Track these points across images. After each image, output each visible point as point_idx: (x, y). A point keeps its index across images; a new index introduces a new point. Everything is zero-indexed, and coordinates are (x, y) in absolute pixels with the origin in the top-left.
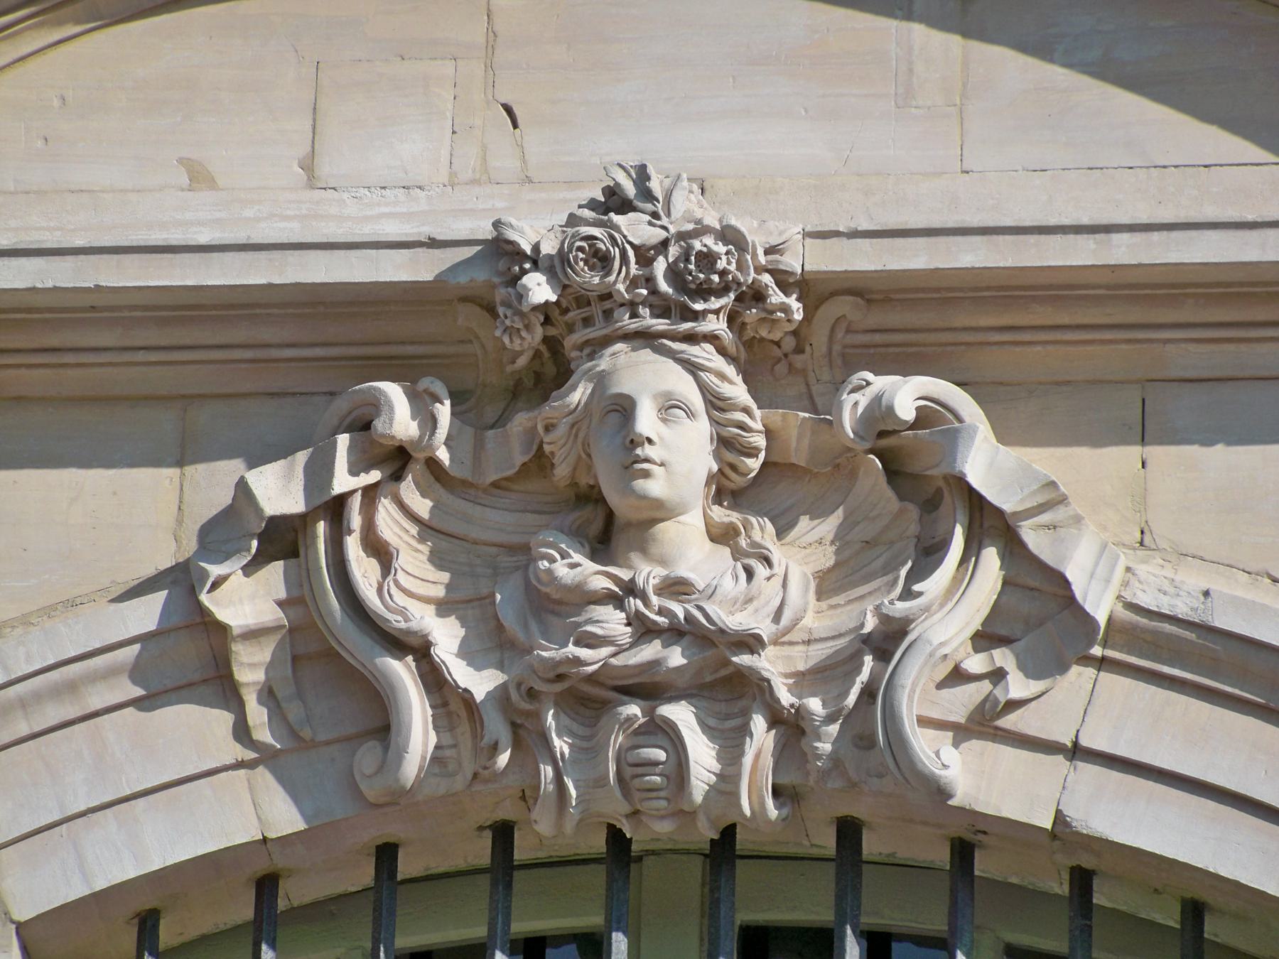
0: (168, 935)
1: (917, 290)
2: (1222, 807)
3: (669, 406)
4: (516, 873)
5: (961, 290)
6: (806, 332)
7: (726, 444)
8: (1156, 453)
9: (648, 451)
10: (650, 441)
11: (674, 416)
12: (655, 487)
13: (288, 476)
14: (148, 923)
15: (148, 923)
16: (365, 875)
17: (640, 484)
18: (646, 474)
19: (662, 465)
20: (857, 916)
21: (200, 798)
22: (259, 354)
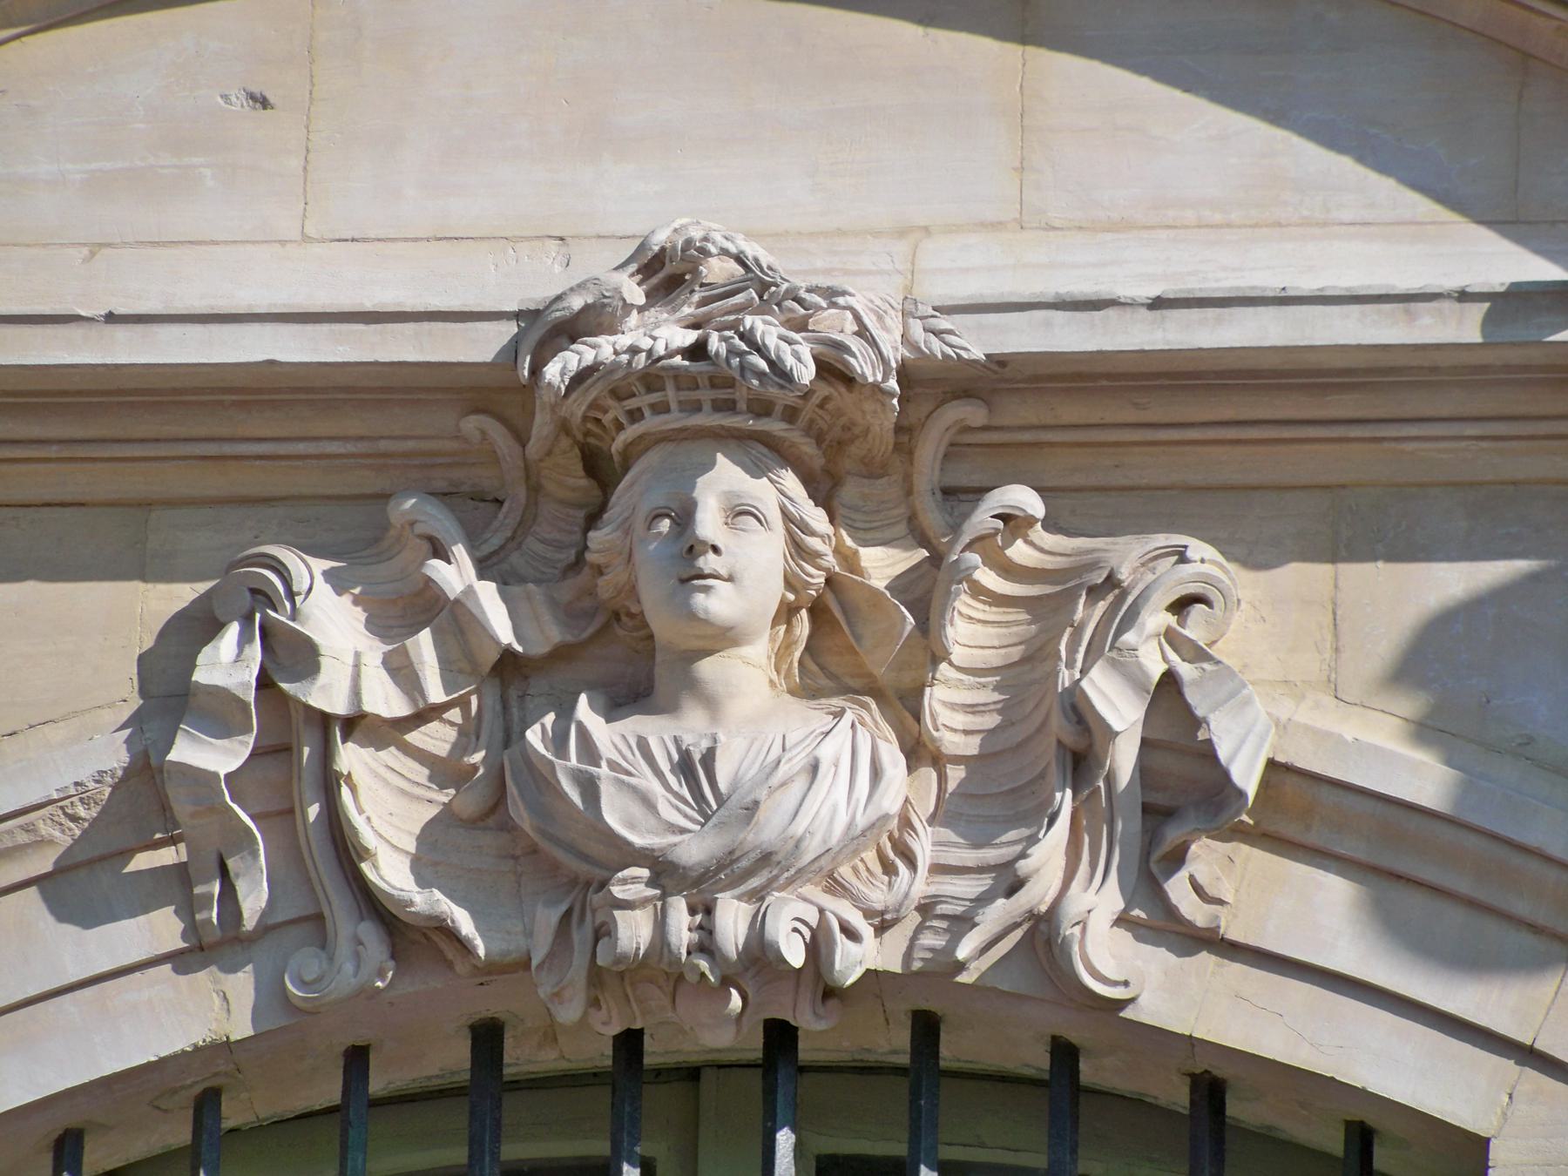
0: (96, 1156)
1: (79, 393)
2: (1504, 1061)
3: (738, 512)
4: (510, 1101)
5: (278, 391)
6: (921, 440)
7: (799, 550)
8: (1342, 567)
9: (708, 562)
10: (715, 549)
11: (751, 534)
12: (717, 603)
13: (246, 685)
14: (68, 1146)
15: (68, 1146)
16: (330, 1091)
17: (700, 600)
18: (707, 590)
19: (730, 579)
20: (934, 1148)
21: (143, 1008)
22: (227, 449)
